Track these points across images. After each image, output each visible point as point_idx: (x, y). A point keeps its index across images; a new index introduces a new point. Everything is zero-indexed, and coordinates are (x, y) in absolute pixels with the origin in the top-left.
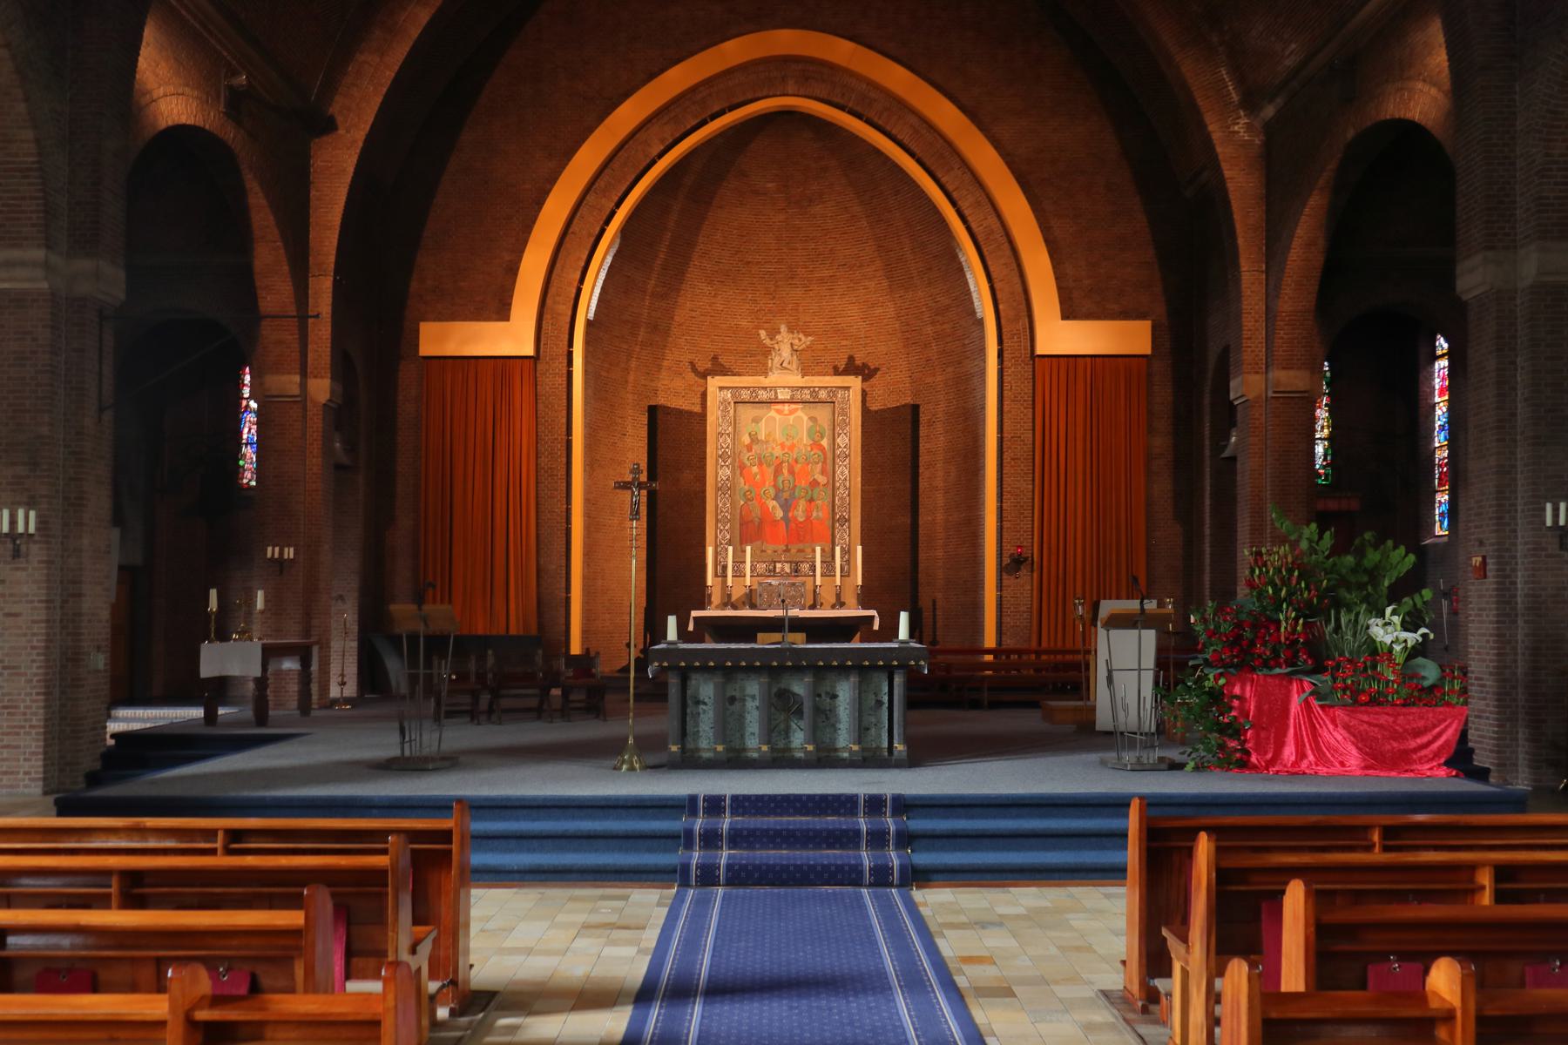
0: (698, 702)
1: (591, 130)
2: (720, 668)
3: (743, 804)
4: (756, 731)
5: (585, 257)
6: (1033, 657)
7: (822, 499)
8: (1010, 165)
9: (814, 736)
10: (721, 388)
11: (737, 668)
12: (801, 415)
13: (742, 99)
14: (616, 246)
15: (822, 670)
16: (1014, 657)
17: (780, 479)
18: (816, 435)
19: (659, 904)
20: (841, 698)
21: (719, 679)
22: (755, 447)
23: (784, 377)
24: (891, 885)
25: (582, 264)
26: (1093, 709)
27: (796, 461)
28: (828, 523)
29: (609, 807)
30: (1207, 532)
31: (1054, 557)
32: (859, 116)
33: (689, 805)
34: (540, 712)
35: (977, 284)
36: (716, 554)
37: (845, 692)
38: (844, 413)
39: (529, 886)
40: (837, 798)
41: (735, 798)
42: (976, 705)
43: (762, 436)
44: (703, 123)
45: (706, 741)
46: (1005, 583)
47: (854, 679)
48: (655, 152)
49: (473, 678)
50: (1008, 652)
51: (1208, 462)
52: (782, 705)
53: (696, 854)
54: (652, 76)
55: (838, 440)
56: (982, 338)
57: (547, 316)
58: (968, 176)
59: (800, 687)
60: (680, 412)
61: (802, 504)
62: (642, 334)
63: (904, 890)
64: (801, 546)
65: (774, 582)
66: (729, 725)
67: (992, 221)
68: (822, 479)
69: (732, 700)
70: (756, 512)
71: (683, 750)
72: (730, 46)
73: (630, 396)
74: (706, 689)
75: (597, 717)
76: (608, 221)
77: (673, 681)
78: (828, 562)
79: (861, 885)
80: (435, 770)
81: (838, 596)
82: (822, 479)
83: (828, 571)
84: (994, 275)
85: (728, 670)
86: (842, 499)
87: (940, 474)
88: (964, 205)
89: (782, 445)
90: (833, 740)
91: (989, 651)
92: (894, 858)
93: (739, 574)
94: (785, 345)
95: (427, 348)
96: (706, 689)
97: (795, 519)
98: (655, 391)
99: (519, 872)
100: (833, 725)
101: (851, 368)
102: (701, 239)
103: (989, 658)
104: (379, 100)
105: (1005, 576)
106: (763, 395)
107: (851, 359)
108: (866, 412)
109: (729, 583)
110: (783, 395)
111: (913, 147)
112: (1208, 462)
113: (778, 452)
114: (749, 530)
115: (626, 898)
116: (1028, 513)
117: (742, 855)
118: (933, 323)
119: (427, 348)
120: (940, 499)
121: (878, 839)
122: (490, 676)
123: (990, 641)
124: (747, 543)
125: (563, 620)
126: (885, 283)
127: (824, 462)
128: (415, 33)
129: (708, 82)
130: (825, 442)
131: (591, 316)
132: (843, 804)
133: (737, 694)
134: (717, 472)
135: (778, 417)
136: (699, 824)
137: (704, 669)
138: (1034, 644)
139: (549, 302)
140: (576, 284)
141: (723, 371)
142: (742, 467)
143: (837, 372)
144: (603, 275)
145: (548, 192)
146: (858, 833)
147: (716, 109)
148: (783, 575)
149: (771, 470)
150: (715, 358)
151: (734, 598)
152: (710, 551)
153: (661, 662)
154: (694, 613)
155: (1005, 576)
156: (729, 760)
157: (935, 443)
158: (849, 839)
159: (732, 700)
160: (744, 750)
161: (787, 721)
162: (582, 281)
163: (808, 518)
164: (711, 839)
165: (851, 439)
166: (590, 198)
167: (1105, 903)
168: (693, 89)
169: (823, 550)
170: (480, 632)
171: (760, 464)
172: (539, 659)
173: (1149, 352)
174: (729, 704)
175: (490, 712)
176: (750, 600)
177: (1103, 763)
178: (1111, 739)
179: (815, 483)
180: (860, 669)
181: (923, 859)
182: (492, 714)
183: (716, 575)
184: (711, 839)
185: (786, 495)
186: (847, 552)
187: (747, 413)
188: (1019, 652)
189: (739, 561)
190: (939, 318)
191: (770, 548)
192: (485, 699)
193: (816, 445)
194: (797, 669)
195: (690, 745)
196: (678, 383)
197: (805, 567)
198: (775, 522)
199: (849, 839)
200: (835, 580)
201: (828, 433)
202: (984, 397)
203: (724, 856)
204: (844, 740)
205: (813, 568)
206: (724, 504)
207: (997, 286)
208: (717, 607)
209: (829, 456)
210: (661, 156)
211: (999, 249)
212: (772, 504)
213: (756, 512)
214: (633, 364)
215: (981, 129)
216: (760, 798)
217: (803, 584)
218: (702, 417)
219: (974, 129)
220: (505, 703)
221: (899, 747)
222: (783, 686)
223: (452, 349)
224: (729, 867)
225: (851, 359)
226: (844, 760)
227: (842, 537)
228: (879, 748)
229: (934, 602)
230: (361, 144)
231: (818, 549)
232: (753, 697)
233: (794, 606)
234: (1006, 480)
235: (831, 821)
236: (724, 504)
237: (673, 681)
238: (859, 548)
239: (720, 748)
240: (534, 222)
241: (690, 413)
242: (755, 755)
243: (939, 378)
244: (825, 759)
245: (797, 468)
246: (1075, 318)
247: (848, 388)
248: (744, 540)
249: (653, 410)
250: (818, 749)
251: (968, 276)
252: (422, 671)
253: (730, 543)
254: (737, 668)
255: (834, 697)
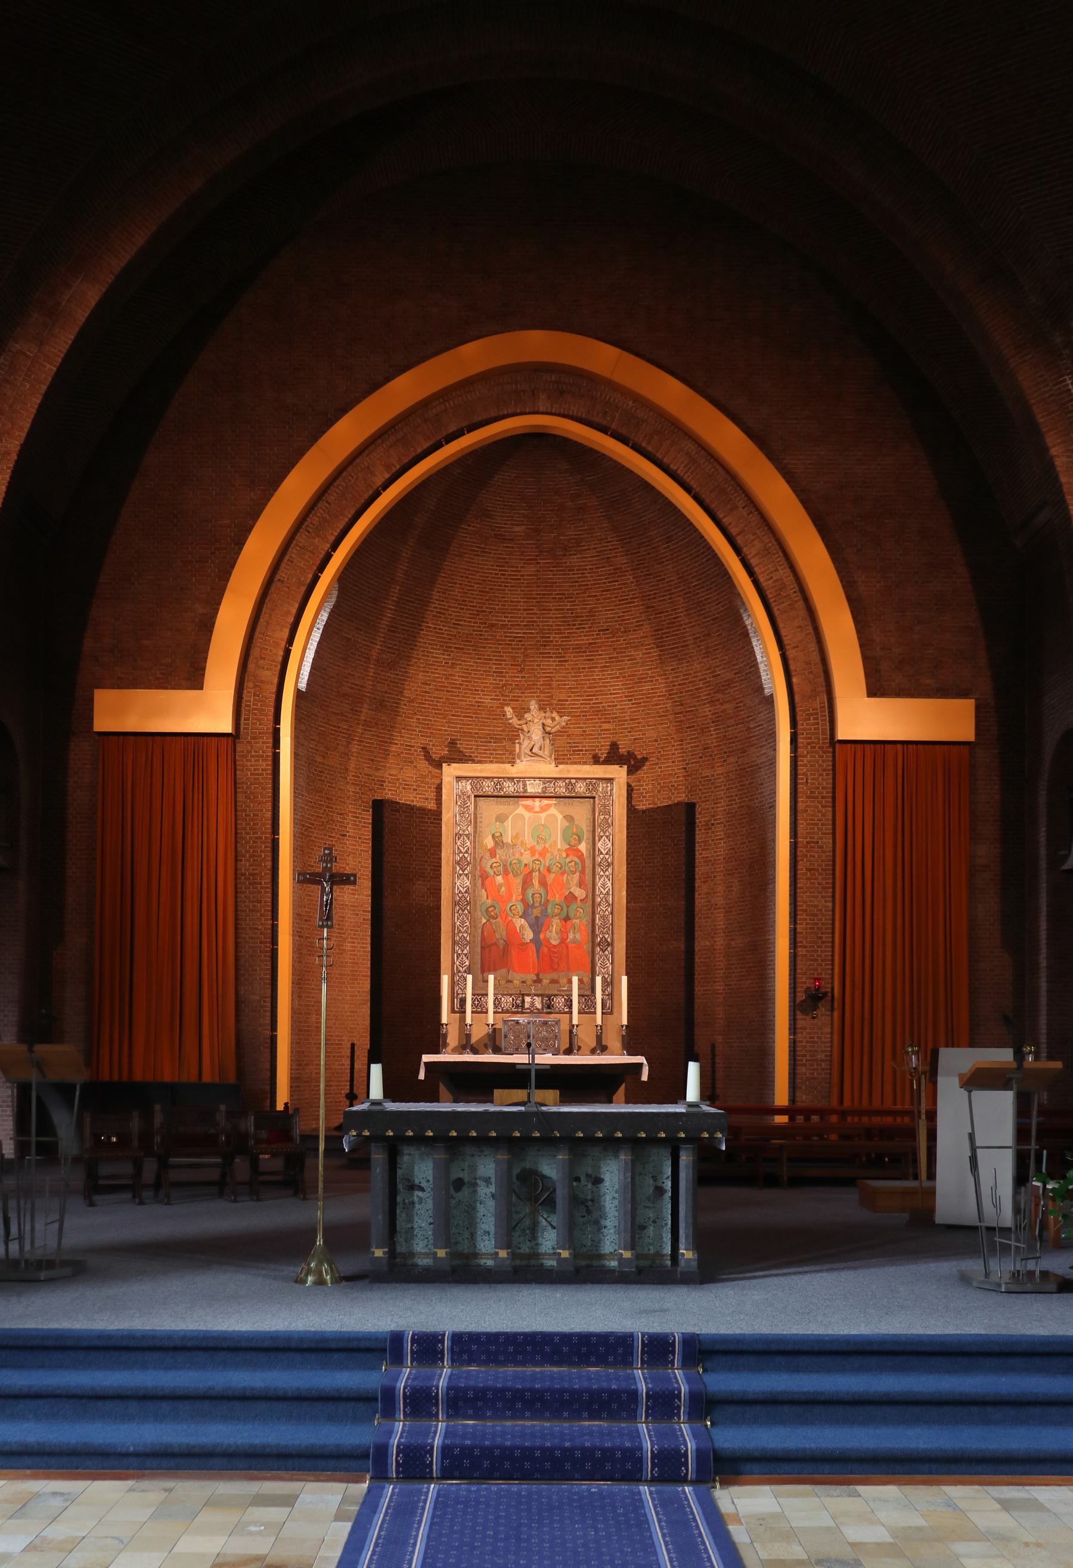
0: (412, 1187)
1: (301, 453)
2: (441, 1140)
3: (471, 1346)
4: (492, 1229)
5: (294, 611)
6: (834, 1119)
7: (580, 918)
8: (806, 503)
9: (570, 1238)
10: (459, 778)
11: (464, 1140)
12: (554, 814)
13: (484, 417)
14: (333, 600)
15: (584, 1142)
16: (815, 1118)
17: (530, 892)
18: (572, 838)
19: (339, 1517)
20: (607, 1183)
21: (441, 1155)
22: (499, 851)
23: (534, 766)
24: (684, 1481)
25: (291, 619)
26: (932, 1193)
27: (549, 870)
28: (587, 947)
29: (277, 1349)
30: (1043, 963)
31: (858, 993)
32: (624, 441)
33: (389, 1348)
34: (222, 1187)
35: (765, 652)
36: (453, 984)
37: (613, 1174)
38: (606, 810)
39: (152, 1477)
40: (604, 1339)
41: (458, 1338)
42: (771, 1181)
43: (508, 839)
44: (437, 446)
45: (423, 1244)
46: (800, 1024)
47: (624, 1157)
48: (379, 481)
49: (135, 1143)
50: (808, 1112)
51: (1044, 876)
52: (527, 1193)
53: (399, 1426)
54: (375, 386)
55: (599, 845)
56: (772, 720)
57: (249, 684)
58: (754, 518)
59: (551, 1167)
60: (411, 808)
61: (556, 924)
62: (365, 712)
63: (703, 1487)
64: (555, 976)
65: (522, 1019)
66: (453, 1220)
67: (784, 573)
68: (580, 893)
69: (459, 1184)
70: (501, 933)
71: (392, 1254)
72: (468, 350)
73: (351, 788)
74: (423, 1169)
75: (296, 1194)
76: (322, 568)
77: (378, 1157)
78: (588, 997)
79: (639, 1480)
80: (49, 1280)
81: (599, 1038)
82: (580, 893)
83: (588, 1008)
84: (786, 641)
85: (453, 1141)
86: (603, 917)
87: (721, 889)
88: (749, 552)
89: (533, 851)
90: (597, 1243)
91: (781, 1111)
92: (687, 1436)
93: (480, 1009)
94: (536, 726)
95: (102, 724)
96: (423, 1169)
97: (547, 941)
98: (382, 782)
99: (136, 1455)
100: (597, 1223)
101: (614, 757)
102: (436, 595)
103: (781, 1119)
104: (37, 400)
105: (799, 1016)
106: (509, 788)
107: (614, 746)
108: (632, 811)
109: (469, 1021)
110: (533, 788)
111: (688, 478)
112: (1044, 876)
113: (527, 858)
114: (492, 956)
115: (288, 1501)
116: (827, 937)
117: (478, 1374)
118: (712, 702)
119: (102, 724)
120: (720, 920)
121: (663, 1404)
122: (158, 1139)
123: (781, 1097)
124: (490, 971)
125: (268, 1066)
126: (655, 652)
127: (583, 872)
128: (82, 315)
129: (443, 395)
130: (583, 847)
131: (303, 685)
132: (611, 1348)
133: (465, 1176)
134: (453, 882)
135: (527, 814)
136: (405, 1377)
137: (420, 1140)
138: (835, 1102)
139: (251, 666)
140: (283, 644)
141: (458, 756)
142: (484, 876)
143: (596, 760)
144: (316, 636)
145: (249, 530)
146: (634, 1395)
147: (452, 428)
148: (532, 1011)
149: (519, 880)
150: (453, 743)
151: (474, 1040)
152: (445, 980)
153: (360, 1130)
154: (426, 1058)
155: (799, 1016)
156: (454, 1270)
157: (713, 848)
158: (619, 1404)
159: (459, 1184)
160: (476, 1255)
161: (534, 1214)
162: (290, 641)
163: (563, 940)
164: (421, 1403)
165: (614, 843)
166: (301, 538)
167: (1004, 1521)
168: (425, 404)
169: (580, 981)
170: (167, 1078)
171: (506, 873)
172: (221, 1118)
173: (971, 737)
174: (455, 1188)
175: (157, 1186)
176: (493, 1042)
177: (965, 1279)
178: (967, 1238)
179: (571, 898)
180: (633, 1143)
181: (731, 1438)
182: (160, 1189)
183: (453, 1011)
184: (421, 1403)
185: (536, 912)
186: (610, 984)
187: (490, 809)
188: (822, 1113)
189: (480, 994)
190: (719, 696)
191: (517, 978)
192: (150, 1168)
193: (573, 850)
194: (548, 1142)
195: (401, 1248)
196: (409, 773)
197: (559, 1002)
198: (523, 945)
199: (619, 1404)
200: (595, 1018)
201: (586, 835)
202: (773, 793)
203: (439, 1432)
204: (611, 1243)
205: (569, 1003)
206: (463, 922)
207: (791, 653)
208: (455, 1051)
209: (588, 863)
210: (386, 486)
211: (793, 609)
212: (519, 922)
213: (501, 933)
214: (355, 748)
215: (770, 459)
216: (493, 1338)
217: (557, 1022)
218: (437, 815)
219: (761, 456)
220: (173, 1176)
221: (687, 1254)
222: (528, 1165)
223: (132, 724)
224: (446, 1450)
225: (614, 746)
226: (612, 1271)
227: (604, 965)
228: (659, 1255)
229: (713, 1046)
230: (14, 457)
231: (575, 980)
232: (487, 1181)
233: (545, 1051)
234: (802, 896)
235: (593, 1375)
236: (463, 922)
237: (378, 1157)
238: (625, 979)
239: (441, 1253)
240: (233, 567)
241: (422, 810)
242: (490, 1263)
243: (720, 770)
244: (585, 1271)
245: (550, 878)
246: (882, 695)
247: (610, 780)
248: (486, 969)
249: (379, 807)
250: (575, 1256)
251: (754, 642)
252: (33, 1139)
253: (469, 971)
254: (464, 1140)
255: (598, 1181)
